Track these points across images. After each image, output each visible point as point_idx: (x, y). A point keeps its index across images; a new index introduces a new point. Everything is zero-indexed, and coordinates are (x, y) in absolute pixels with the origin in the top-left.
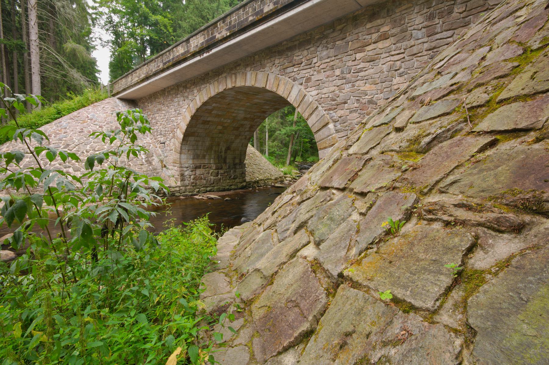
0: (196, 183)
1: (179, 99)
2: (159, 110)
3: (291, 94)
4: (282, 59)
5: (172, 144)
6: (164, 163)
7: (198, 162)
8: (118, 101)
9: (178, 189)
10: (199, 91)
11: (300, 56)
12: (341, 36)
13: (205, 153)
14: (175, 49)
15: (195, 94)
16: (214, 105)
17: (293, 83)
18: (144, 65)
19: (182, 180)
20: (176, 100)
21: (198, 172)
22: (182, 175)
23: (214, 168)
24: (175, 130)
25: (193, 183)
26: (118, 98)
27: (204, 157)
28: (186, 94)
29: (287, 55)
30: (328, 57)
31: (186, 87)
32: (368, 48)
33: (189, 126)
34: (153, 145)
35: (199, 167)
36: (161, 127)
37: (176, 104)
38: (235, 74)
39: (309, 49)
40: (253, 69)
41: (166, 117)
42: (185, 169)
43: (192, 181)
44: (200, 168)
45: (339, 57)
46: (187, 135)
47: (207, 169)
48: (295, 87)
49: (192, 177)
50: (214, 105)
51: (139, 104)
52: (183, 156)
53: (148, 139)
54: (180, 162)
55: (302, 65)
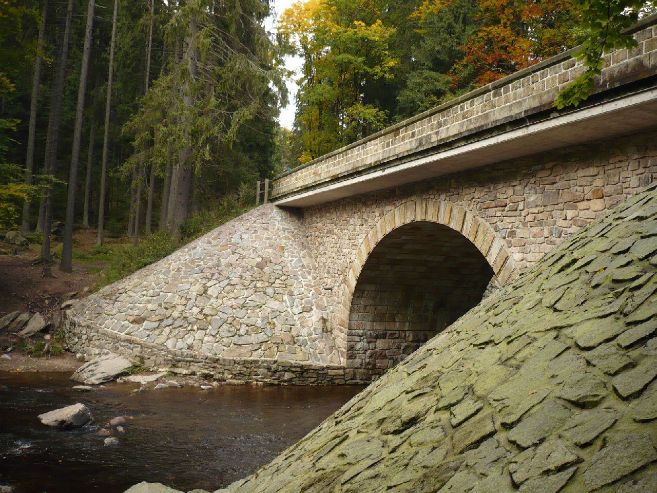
0: (374, 365)
1: (355, 220)
2: (330, 232)
3: (492, 250)
4: (483, 194)
5: (341, 293)
6: (328, 324)
7: (378, 327)
8: (274, 207)
9: (341, 372)
10: (382, 215)
11: (505, 193)
12: (551, 178)
13: (395, 312)
14: (349, 151)
15: (376, 219)
16: (404, 237)
17: (495, 233)
18: (313, 164)
19: (351, 357)
20: (352, 221)
21: (380, 344)
22: (351, 348)
23: (411, 339)
24: (347, 270)
25: (369, 364)
26: (276, 206)
27: (392, 319)
28: (365, 216)
29: (489, 188)
30: (537, 206)
31: (365, 204)
32: (581, 205)
33: (367, 267)
34: (316, 290)
35: (384, 336)
36: (329, 260)
37: (351, 228)
38: (426, 200)
39: (515, 186)
40: (448, 199)
41: (338, 245)
42: (357, 339)
43: (367, 360)
44: (384, 338)
45: (549, 208)
46: (362, 280)
47: (397, 341)
48: (496, 241)
49: (368, 353)
50: (404, 237)
51: (306, 216)
52: (355, 316)
53: (310, 278)
54: (350, 324)
55: (507, 209)
